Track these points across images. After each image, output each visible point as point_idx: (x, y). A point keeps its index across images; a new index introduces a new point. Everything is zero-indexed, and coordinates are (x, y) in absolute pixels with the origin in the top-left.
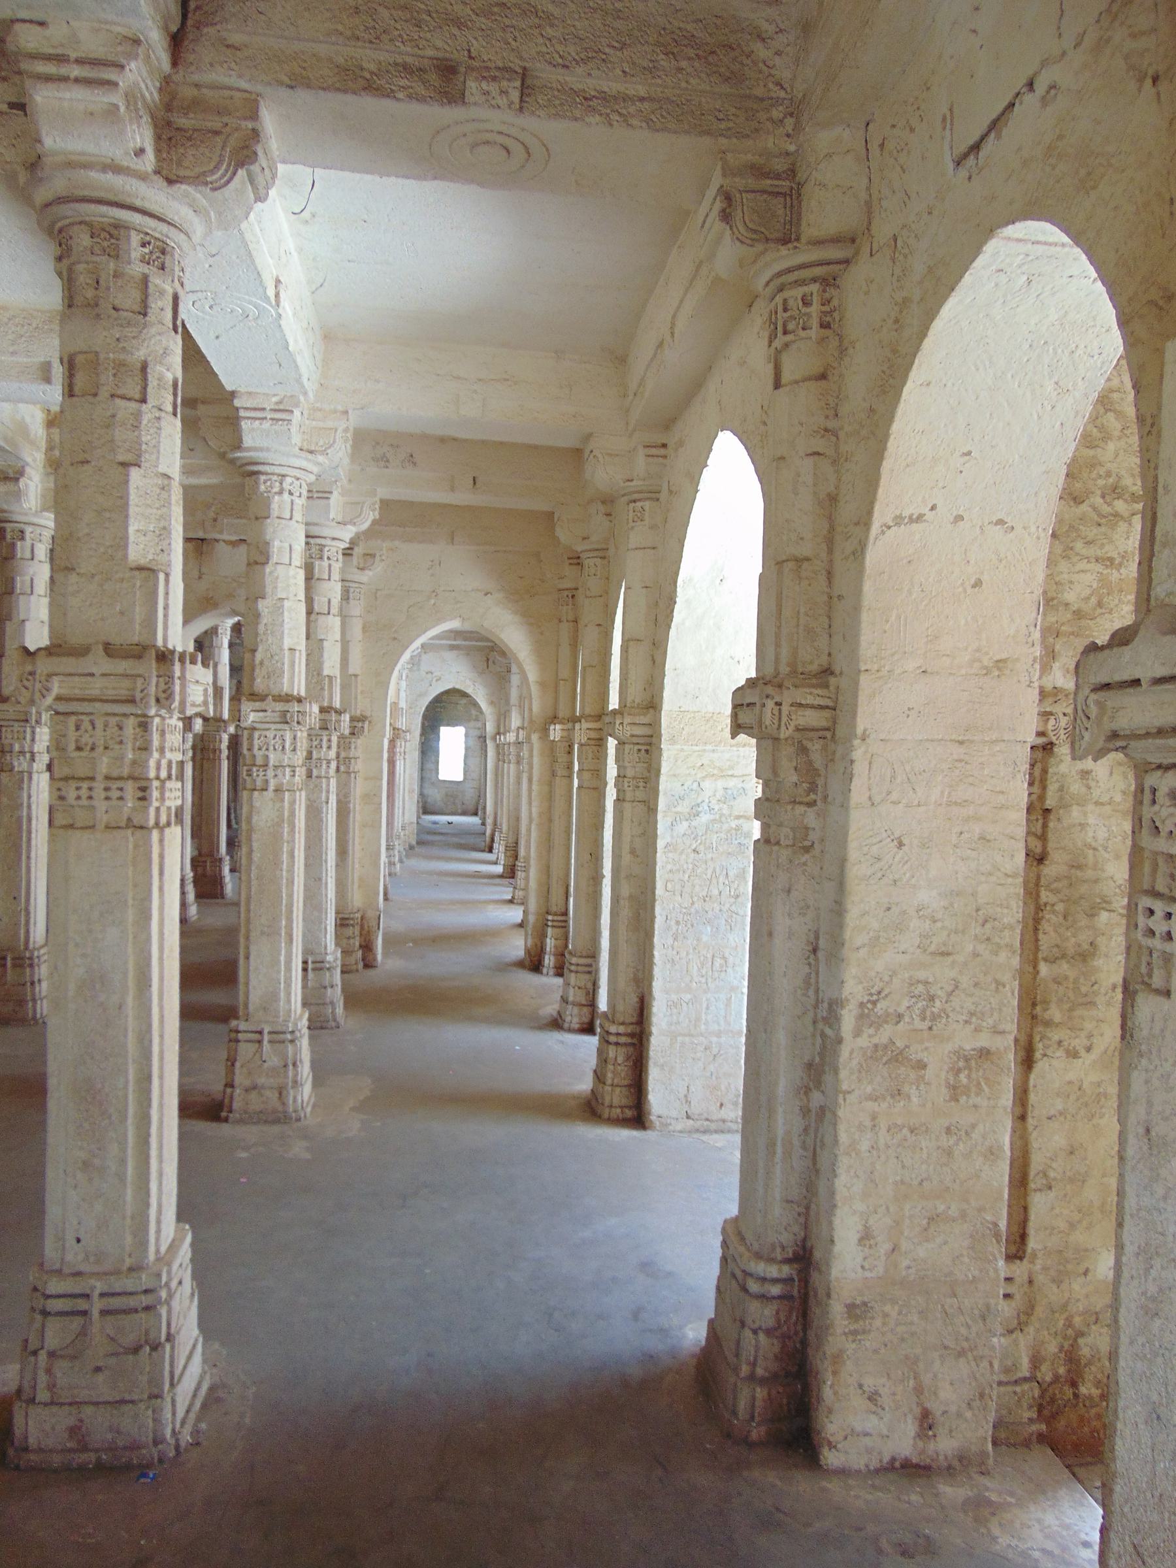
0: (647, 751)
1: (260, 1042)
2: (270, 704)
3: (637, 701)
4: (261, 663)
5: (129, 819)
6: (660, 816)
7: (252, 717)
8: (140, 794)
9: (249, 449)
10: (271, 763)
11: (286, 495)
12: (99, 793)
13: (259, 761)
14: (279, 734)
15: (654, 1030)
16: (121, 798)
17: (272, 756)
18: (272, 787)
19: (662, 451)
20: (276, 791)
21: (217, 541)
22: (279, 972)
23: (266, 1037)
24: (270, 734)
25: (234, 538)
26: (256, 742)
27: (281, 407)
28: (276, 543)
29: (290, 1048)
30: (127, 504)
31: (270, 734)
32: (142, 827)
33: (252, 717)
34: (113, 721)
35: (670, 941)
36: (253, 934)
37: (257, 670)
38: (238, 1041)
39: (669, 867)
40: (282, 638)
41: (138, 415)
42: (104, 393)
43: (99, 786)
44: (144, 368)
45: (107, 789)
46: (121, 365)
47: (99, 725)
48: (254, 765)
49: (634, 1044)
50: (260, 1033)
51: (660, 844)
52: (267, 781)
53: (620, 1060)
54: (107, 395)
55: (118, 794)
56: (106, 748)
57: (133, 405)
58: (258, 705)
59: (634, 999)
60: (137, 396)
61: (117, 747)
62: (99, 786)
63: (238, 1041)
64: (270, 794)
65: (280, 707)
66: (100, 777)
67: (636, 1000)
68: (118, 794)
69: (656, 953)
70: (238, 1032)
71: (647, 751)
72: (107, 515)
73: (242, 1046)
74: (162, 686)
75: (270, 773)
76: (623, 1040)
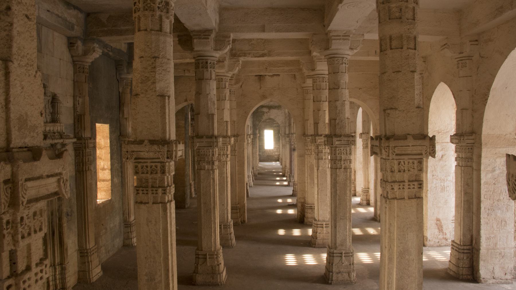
0: (471, 148)
1: (341, 257)
2: (343, 138)
3: (468, 131)
4: (338, 124)
5: (415, 195)
6: (482, 172)
7: (337, 143)
8: (419, 186)
9: (333, 50)
10: (343, 159)
11: (344, 64)
12: (406, 186)
13: (338, 158)
14: (345, 148)
15: (481, 248)
16: (414, 188)
17: (343, 156)
18: (343, 167)
19: (476, 43)
20: (344, 169)
21: (266, 75)
22: (347, 232)
23: (343, 255)
24: (342, 149)
25: (271, 74)
26: (337, 152)
27: (346, 35)
28: (342, 81)
29: (352, 259)
30: (414, 85)
31: (342, 149)
32: (419, 198)
33: (319, 141)
34: (411, 161)
35: (486, 216)
36: (337, 219)
37: (337, 126)
38: (334, 256)
39: (485, 190)
40: (345, 115)
41: (415, 54)
42: (405, 48)
43: (406, 184)
44: (415, 38)
45: (409, 185)
46: (409, 37)
47: (406, 163)
48: (336, 160)
49: (470, 253)
50: (341, 253)
51: (482, 182)
52: (341, 165)
53: (465, 258)
54: (406, 48)
55: (413, 186)
56: (409, 171)
57: (414, 51)
58: (338, 139)
59: (469, 237)
60: (413, 48)
61: (412, 170)
62: (406, 184)
63: (334, 256)
64: (342, 170)
65: (346, 139)
66: (406, 181)
67: (469, 237)
68: (413, 186)
69: (481, 221)
70: (333, 253)
71: (471, 148)
72: (408, 89)
73: (335, 258)
74: (431, 149)
75: (342, 162)
76: (466, 251)
